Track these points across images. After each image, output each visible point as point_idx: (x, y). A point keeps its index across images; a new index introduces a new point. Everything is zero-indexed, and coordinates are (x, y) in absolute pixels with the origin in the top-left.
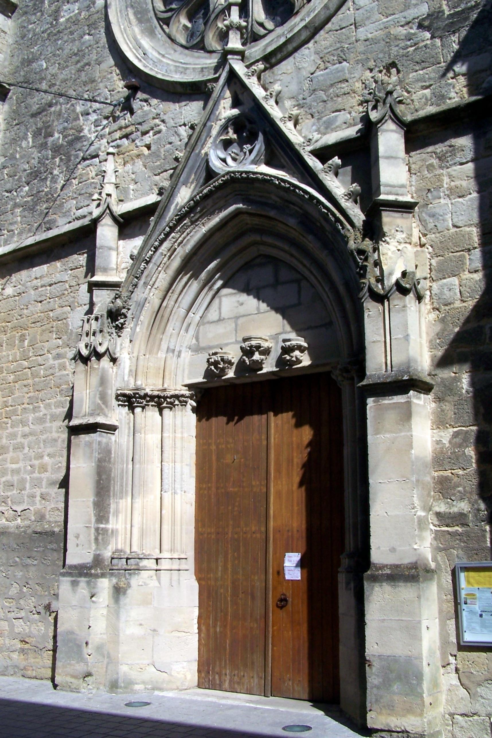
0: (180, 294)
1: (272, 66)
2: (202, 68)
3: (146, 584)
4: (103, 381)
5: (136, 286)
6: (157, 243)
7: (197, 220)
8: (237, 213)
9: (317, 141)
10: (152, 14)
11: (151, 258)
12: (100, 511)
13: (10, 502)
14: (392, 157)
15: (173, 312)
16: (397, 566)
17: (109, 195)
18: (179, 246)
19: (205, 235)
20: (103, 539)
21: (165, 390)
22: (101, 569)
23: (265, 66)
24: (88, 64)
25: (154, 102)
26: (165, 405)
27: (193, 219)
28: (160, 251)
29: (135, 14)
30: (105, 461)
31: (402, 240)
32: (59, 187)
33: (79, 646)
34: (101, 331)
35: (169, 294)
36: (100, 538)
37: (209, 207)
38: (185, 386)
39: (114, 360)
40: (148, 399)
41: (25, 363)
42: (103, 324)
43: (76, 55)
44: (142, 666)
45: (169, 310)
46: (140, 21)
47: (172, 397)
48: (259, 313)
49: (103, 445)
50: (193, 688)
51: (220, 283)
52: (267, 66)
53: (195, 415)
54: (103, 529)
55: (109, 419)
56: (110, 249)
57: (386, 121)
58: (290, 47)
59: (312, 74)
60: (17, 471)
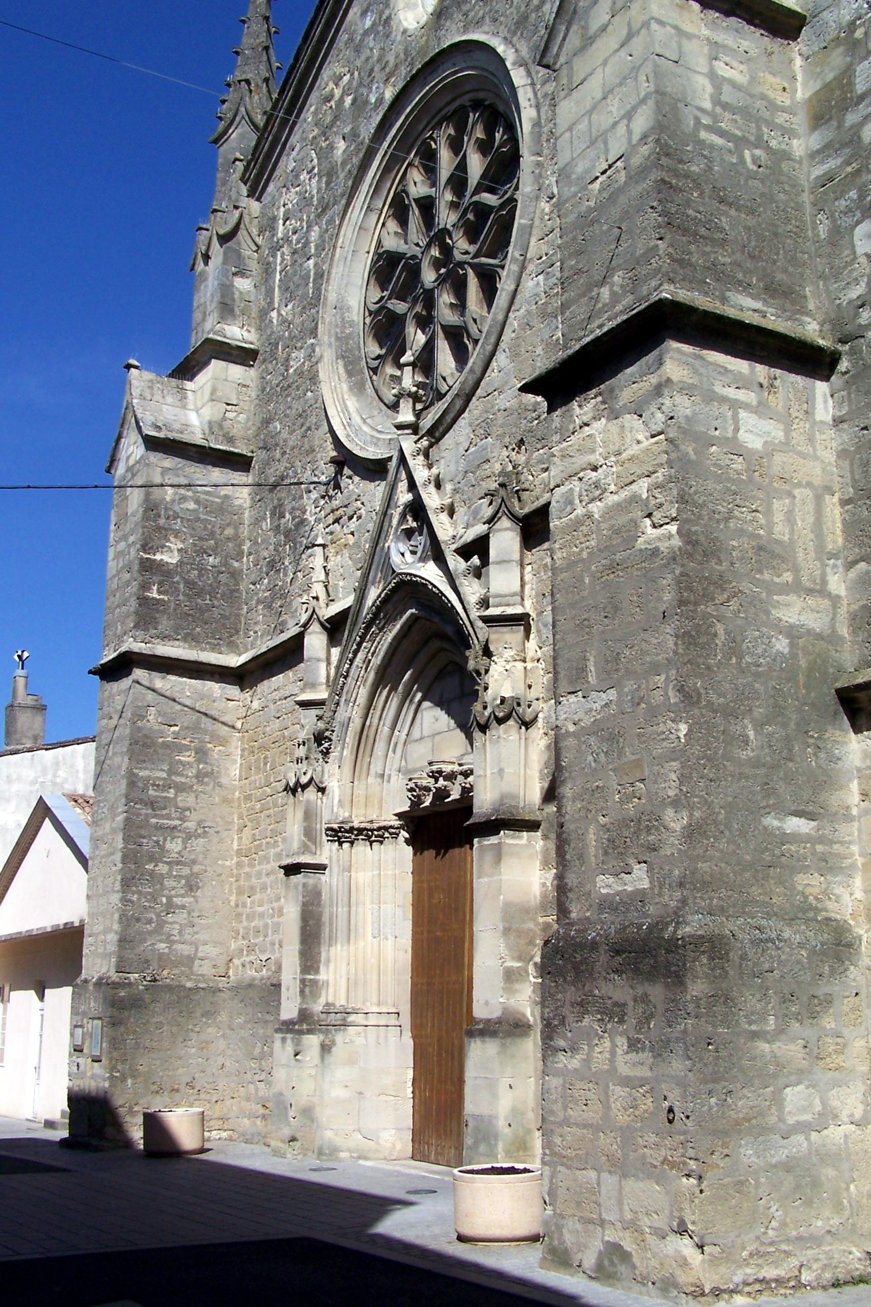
0: (383, 710)
1: (438, 440)
2: (390, 440)
3: (352, 1042)
4: (309, 815)
5: (338, 704)
6: (351, 655)
7: (383, 627)
8: (413, 619)
9: (461, 538)
10: (364, 363)
11: (348, 672)
12: (307, 960)
13: (257, 950)
14: (504, 561)
15: (379, 731)
16: (489, 1020)
17: (316, 598)
18: (372, 656)
19: (391, 644)
20: (311, 992)
21: (371, 822)
22: (308, 1024)
23: (430, 441)
24: (309, 429)
25: (357, 479)
26: (373, 838)
27: (380, 626)
28: (355, 663)
29: (345, 366)
30: (312, 904)
31: (510, 659)
32: (289, 581)
33: (286, 1108)
34: (306, 758)
35: (371, 711)
36: (307, 990)
37: (391, 612)
38: (396, 815)
39: (322, 790)
40: (355, 832)
41: (268, 790)
42: (309, 749)
43: (300, 416)
44: (348, 1132)
45: (373, 729)
46: (350, 374)
47: (379, 829)
48: (449, 730)
49: (310, 888)
50: (405, 1159)
51: (419, 696)
52: (433, 440)
53: (411, 848)
54: (311, 980)
55: (317, 856)
56: (319, 660)
57: (500, 518)
58: (449, 419)
59: (466, 451)
60: (262, 915)
